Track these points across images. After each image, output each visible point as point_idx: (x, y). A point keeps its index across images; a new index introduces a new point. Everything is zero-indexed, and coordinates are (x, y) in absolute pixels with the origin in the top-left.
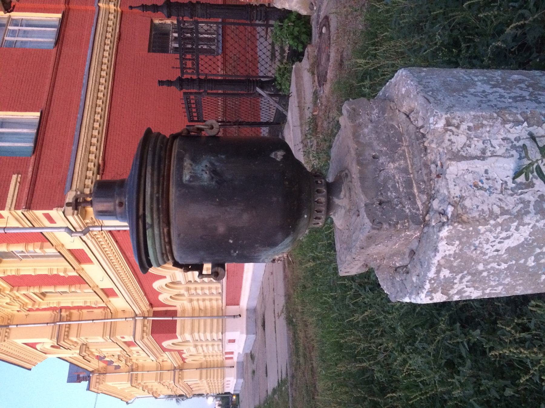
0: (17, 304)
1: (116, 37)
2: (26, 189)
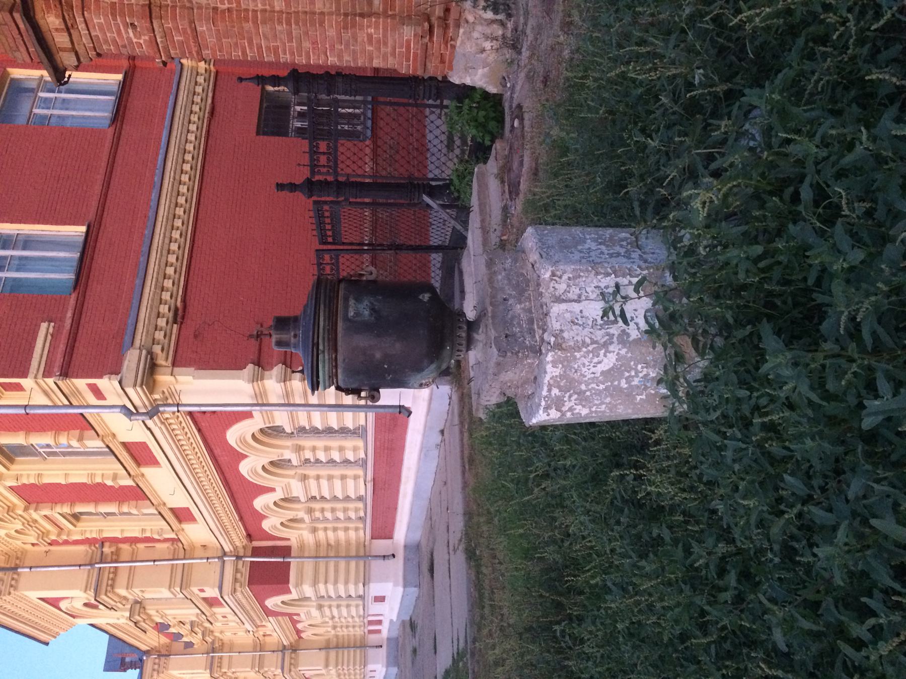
0: (33, 533)
1: (207, 111)
2: (62, 346)
